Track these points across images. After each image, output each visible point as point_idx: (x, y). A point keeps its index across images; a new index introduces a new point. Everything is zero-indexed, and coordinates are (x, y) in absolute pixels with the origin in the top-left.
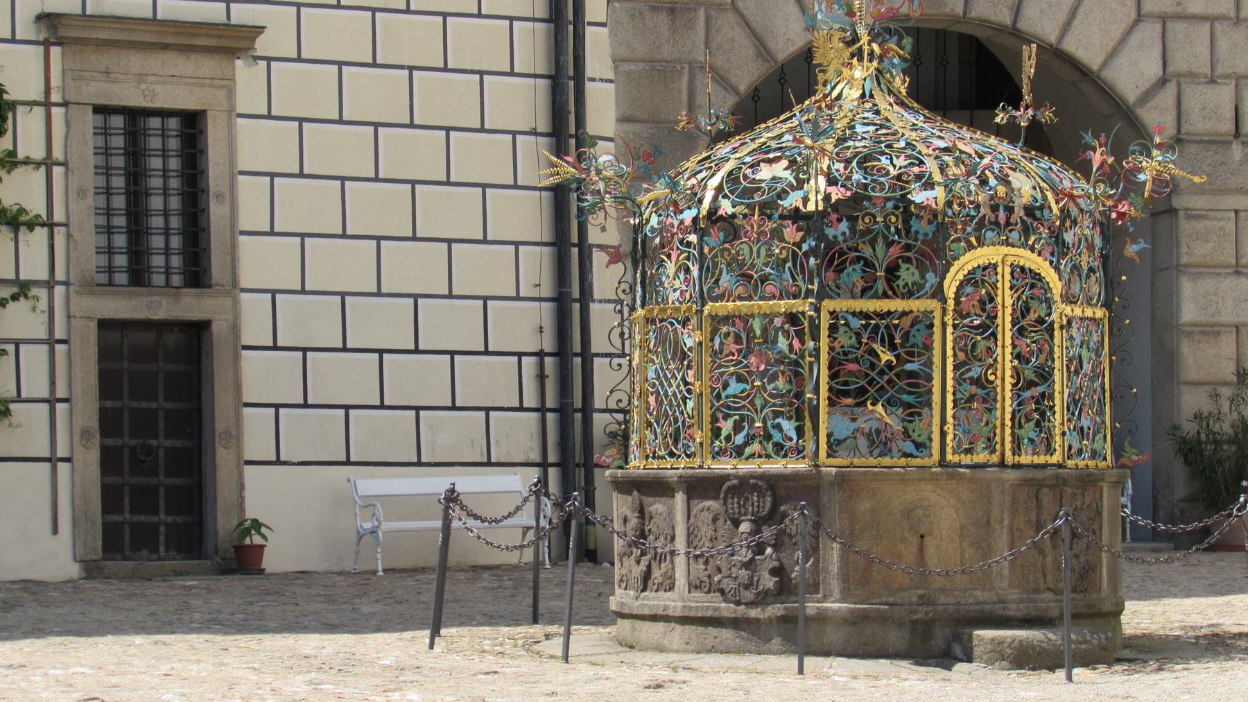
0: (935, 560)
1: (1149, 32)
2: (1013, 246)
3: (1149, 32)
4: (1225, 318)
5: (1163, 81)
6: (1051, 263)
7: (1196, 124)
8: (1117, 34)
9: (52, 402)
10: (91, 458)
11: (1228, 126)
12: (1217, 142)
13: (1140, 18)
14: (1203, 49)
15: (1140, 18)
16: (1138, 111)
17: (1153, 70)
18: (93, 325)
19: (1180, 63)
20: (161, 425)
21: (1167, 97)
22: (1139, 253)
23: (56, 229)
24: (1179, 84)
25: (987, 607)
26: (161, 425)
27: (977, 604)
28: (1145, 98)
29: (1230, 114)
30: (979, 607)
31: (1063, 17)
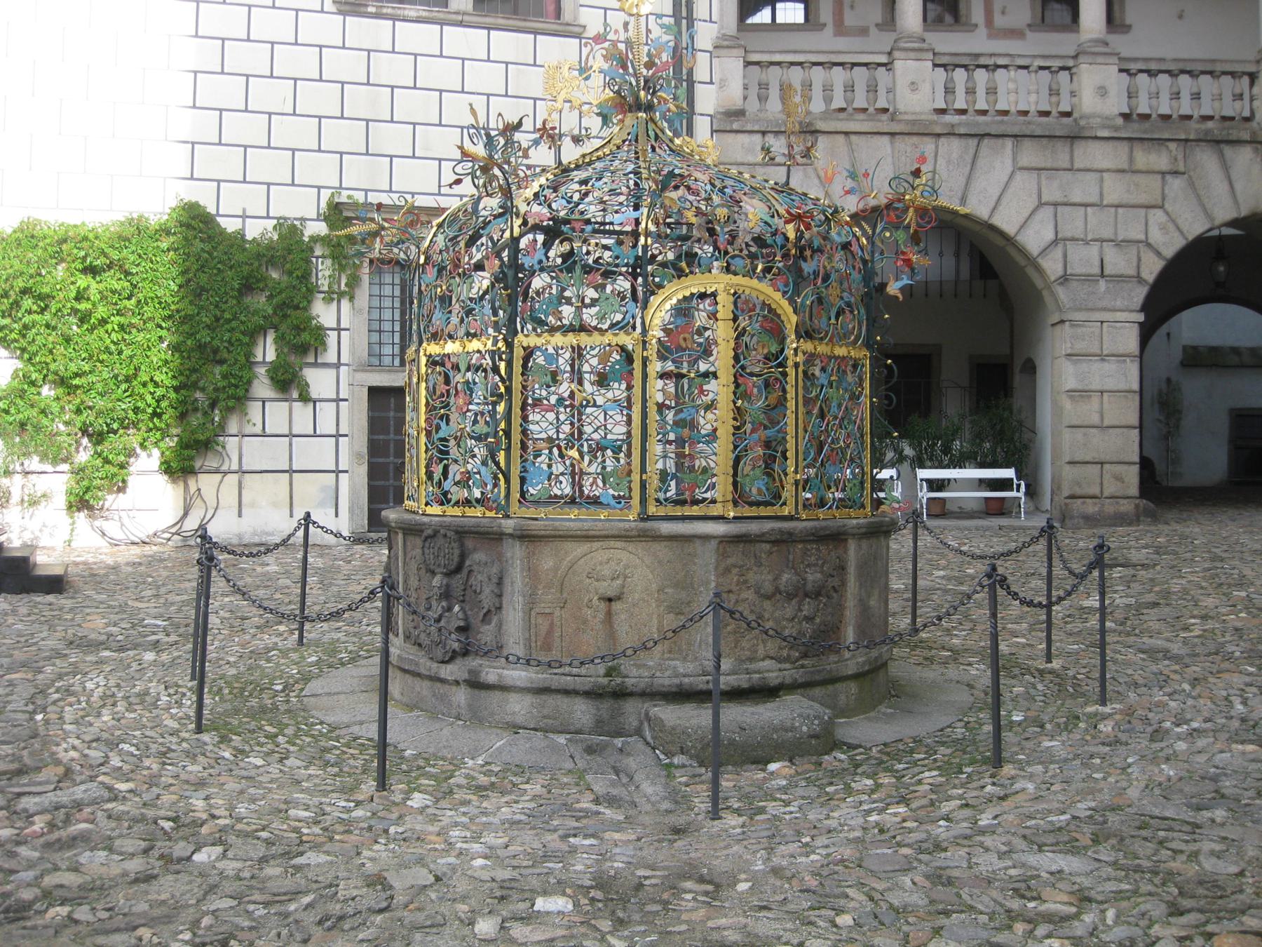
0: (626, 627)
1: (1047, 212)
2: (735, 274)
3: (1047, 212)
4: (1093, 387)
5: (1055, 242)
6: (785, 293)
7: (1076, 268)
8: (1026, 215)
9: (338, 436)
10: (363, 470)
11: (1097, 270)
12: (1088, 279)
13: (1041, 204)
14: (1080, 223)
15: (1041, 204)
16: (1040, 260)
17: (1049, 235)
18: (366, 390)
19: (1066, 232)
20: (392, 450)
21: (1058, 253)
22: (902, 289)
23: (343, 333)
24: (1065, 245)
25: (686, 680)
26: (392, 450)
27: (676, 676)
28: (1044, 251)
29: (1097, 263)
30: (676, 681)
31: (992, 204)
